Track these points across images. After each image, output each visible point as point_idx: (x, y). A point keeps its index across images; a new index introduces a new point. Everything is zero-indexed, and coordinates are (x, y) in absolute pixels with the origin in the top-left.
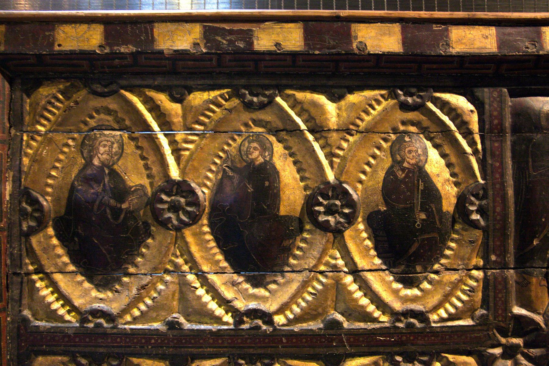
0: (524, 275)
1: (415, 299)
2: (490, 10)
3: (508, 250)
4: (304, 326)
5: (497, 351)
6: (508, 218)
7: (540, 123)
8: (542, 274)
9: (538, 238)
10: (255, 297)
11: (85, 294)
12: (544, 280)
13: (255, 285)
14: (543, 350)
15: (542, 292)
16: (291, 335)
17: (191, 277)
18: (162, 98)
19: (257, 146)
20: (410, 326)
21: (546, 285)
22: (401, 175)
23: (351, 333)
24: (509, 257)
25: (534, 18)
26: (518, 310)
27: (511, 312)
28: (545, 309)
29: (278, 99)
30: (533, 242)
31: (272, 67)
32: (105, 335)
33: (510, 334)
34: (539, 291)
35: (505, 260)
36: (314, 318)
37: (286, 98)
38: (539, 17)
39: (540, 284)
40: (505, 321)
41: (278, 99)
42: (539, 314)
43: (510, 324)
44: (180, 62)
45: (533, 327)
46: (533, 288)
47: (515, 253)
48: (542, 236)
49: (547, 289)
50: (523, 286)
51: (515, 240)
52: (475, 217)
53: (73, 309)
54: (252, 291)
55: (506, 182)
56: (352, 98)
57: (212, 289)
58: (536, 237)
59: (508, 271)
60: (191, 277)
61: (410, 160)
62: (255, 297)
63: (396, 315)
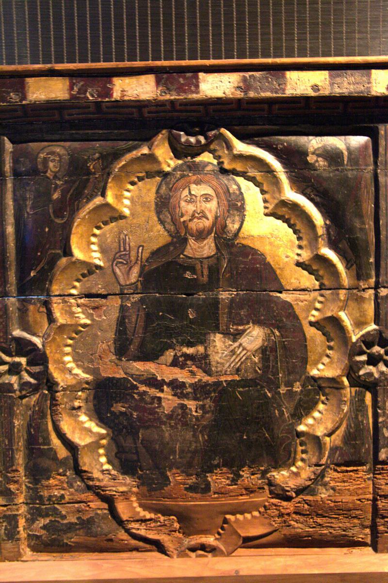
0: (24, 303)
2: (360, 55)
3: (8, 281)
5: (364, 358)
6: (7, 253)
7: (37, 167)
8: (40, 302)
9: (35, 269)
12: (43, 307)
14: (41, 367)
15: (40, 318)
19: (210, 191)
21: (45, 311)
24: (9, 287)
25: (16, 71)
26: (17, 333)
27: (12, 335)
28: (44, 332)
30: (30, 274)
31: (114, 113)
33: (14, 354)
34: (38, 317)
35: (5, 290)
38: (20, 69)
39: (38, 310)
40: (7, 342)
42: (39, 336)
43: (10, 345)
44: (212, 107)
45: (31, 347)
46: (30, 314)
47: (17, 283)
48: (39, 268)
49: (46, 315)
50: (23, 312)
51: (16, 273)
55: (5, 221)
58: (33, 270)
59: (8, 299)
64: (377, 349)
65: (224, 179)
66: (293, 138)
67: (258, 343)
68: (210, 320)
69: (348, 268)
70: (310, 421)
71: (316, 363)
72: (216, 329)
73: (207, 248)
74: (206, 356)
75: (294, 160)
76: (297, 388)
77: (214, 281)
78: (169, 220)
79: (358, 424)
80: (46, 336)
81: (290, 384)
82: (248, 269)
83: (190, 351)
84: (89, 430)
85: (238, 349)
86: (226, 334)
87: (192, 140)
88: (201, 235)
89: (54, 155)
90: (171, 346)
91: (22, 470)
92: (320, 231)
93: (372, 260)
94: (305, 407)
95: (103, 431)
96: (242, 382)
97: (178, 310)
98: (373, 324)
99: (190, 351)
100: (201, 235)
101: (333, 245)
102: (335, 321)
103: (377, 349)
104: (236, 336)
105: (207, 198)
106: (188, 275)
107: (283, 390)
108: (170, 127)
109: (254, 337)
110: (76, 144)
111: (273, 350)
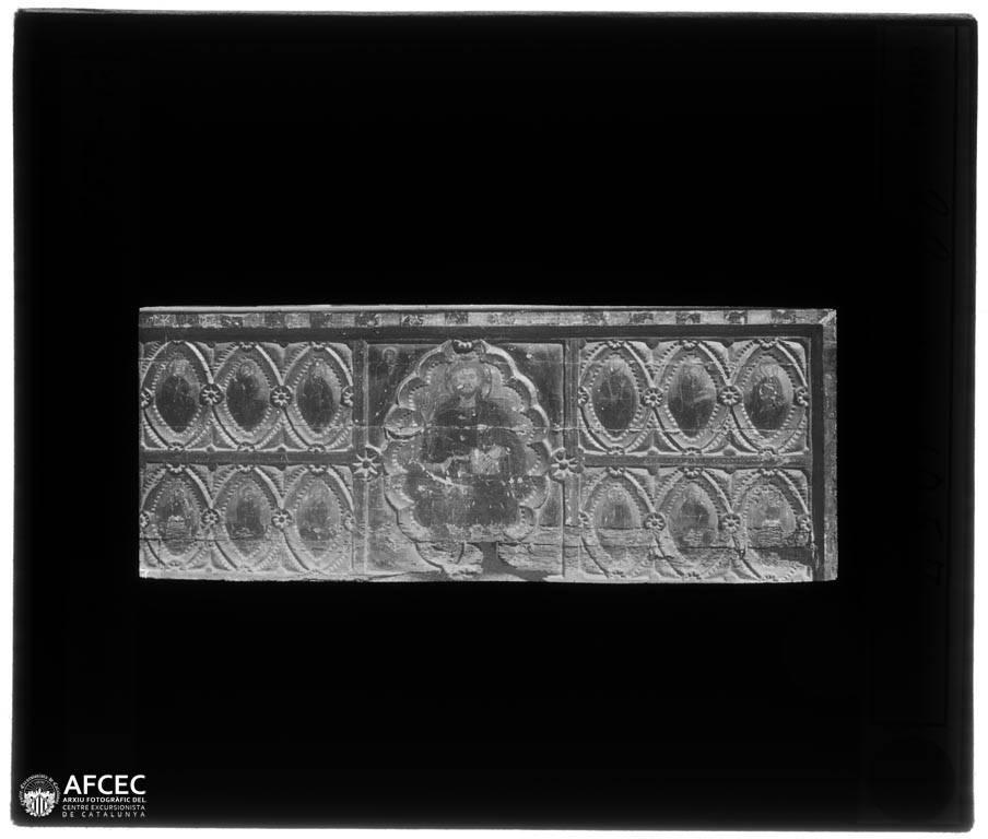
1: (693, 443)
4: (269, 450)
5: (557, 465)
10: (245, 437)
11: (172, 436)
13: (247, 431)
16: (263, 454)
17: (218, 428)
18: (204, 346)
20: (316, 451)
22: (313, 382)
23: (290, 454)
26: (368, 445)
29: (257, 347)
32: (179, 453)
36: (797, 450)
37: (261, 346)
41: (257, 347)
52: (802, 402)
53: (236, 443)
54: (246, 433)
56: (291, 345)
57: (228, 433)
60: (218, 428)
61: (317, 375)
62: (245, 437)
63: (311, 446)
64: (565, 461)
65: (481, 365)
66: (519, 345)
67: (498, 456)
68: (473, 441)
69: (548, 414)
70: (527, 500)
71: (532, 466)
72: (475, 446)
73: (472, 403)
74: (469, 461)
75: (519, 356)
76: (520, 480)
77: (474, 422)
78: (451, 388)
79: (554, 503)
80: (693, 537)
81: (516, 479)
82: (491, 411)
83: (461, 458)
84: (404, 501)
85: (484, 460)
86: (481, 449)
87: (465, 345)
88: (468, 396)
89: (390, 350)
90: (452, 455)
91: (367, 521)
92: (534, 395)
93: (562, 412)
94: (523, 491)
95: (413, 502)
96: (258, 461)
97: (455, 435)
98: (825, 325)
99: (461, 458)
100: (468, 396)
101: (541, 403)
102: (541, 445)
103: (565, 461)
104: (486, 451)
105: (471, 376)
106: (461, 417)
107: (512, 481)
108: (453, 338)
109: (496, 452)
110: (403, 346)
111: (506, 459)
